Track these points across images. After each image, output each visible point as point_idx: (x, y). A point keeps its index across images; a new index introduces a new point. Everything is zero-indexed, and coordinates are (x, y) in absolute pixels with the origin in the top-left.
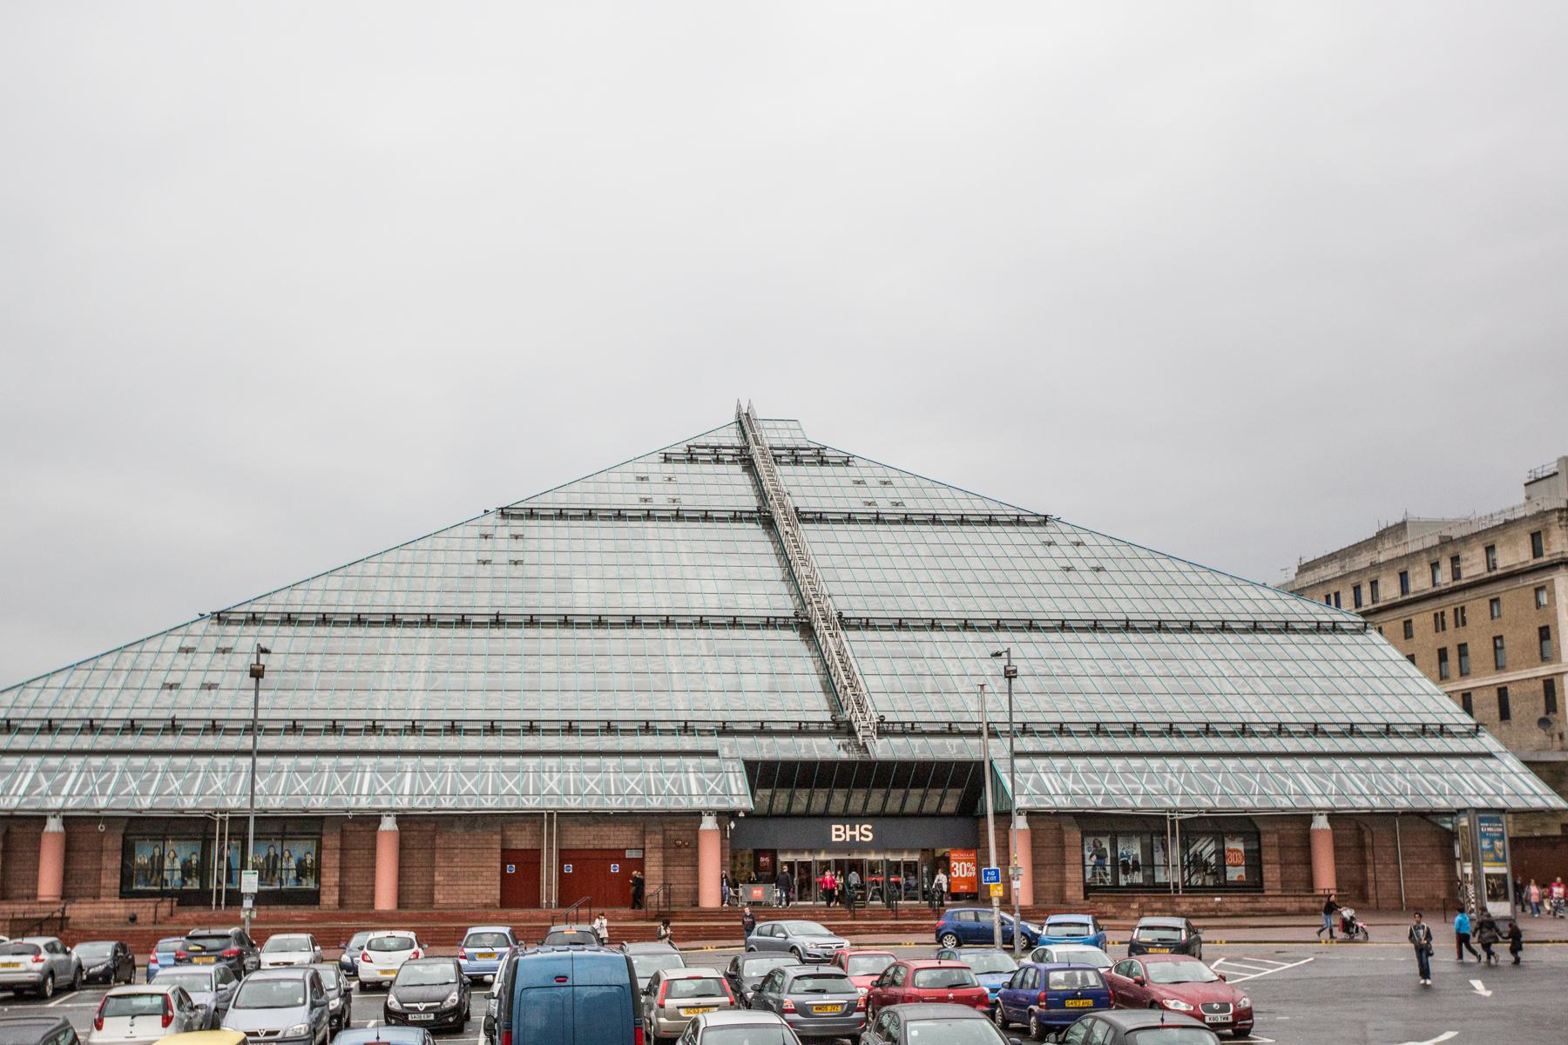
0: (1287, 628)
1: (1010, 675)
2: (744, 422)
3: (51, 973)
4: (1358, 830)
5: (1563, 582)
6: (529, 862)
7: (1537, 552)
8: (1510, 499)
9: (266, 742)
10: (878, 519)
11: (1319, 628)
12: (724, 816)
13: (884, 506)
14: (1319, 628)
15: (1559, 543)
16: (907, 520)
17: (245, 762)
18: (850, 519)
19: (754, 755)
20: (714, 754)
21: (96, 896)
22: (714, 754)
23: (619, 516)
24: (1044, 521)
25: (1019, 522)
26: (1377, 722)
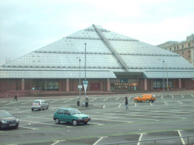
0: (171, 56)
1: (80, 60)
2: (93, 26)
3: (42, 107)
4: (184, 80)
5: (192, 50)
6: (71, 89)
7: (189, 46)
8: (184, 39)
9: (81, 69)
10: (87, 39)
11: (175, 56)
12: (110, 79)
13: (87, 37)
14: (175, 56)
15: (191, 45)
16: (91, 39)
17: (79, 72)
18: (83, 38)
19: (114, 71)
20: (109, 71)
21: (100, 90)
22: (109, 71)
23: (124, 40)
24: (137, 41)
25: (131, 40)
26: (179, 67)
